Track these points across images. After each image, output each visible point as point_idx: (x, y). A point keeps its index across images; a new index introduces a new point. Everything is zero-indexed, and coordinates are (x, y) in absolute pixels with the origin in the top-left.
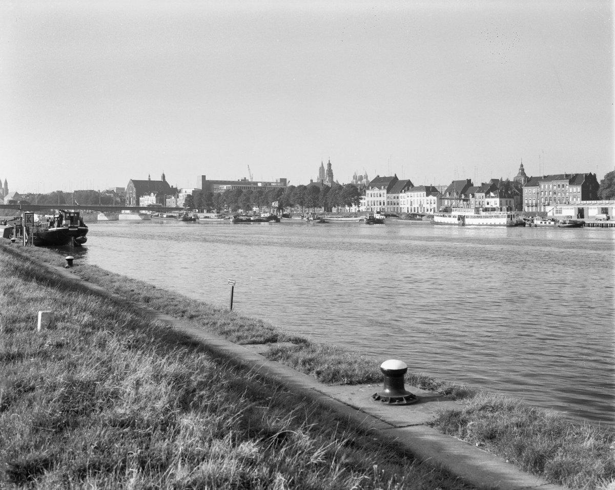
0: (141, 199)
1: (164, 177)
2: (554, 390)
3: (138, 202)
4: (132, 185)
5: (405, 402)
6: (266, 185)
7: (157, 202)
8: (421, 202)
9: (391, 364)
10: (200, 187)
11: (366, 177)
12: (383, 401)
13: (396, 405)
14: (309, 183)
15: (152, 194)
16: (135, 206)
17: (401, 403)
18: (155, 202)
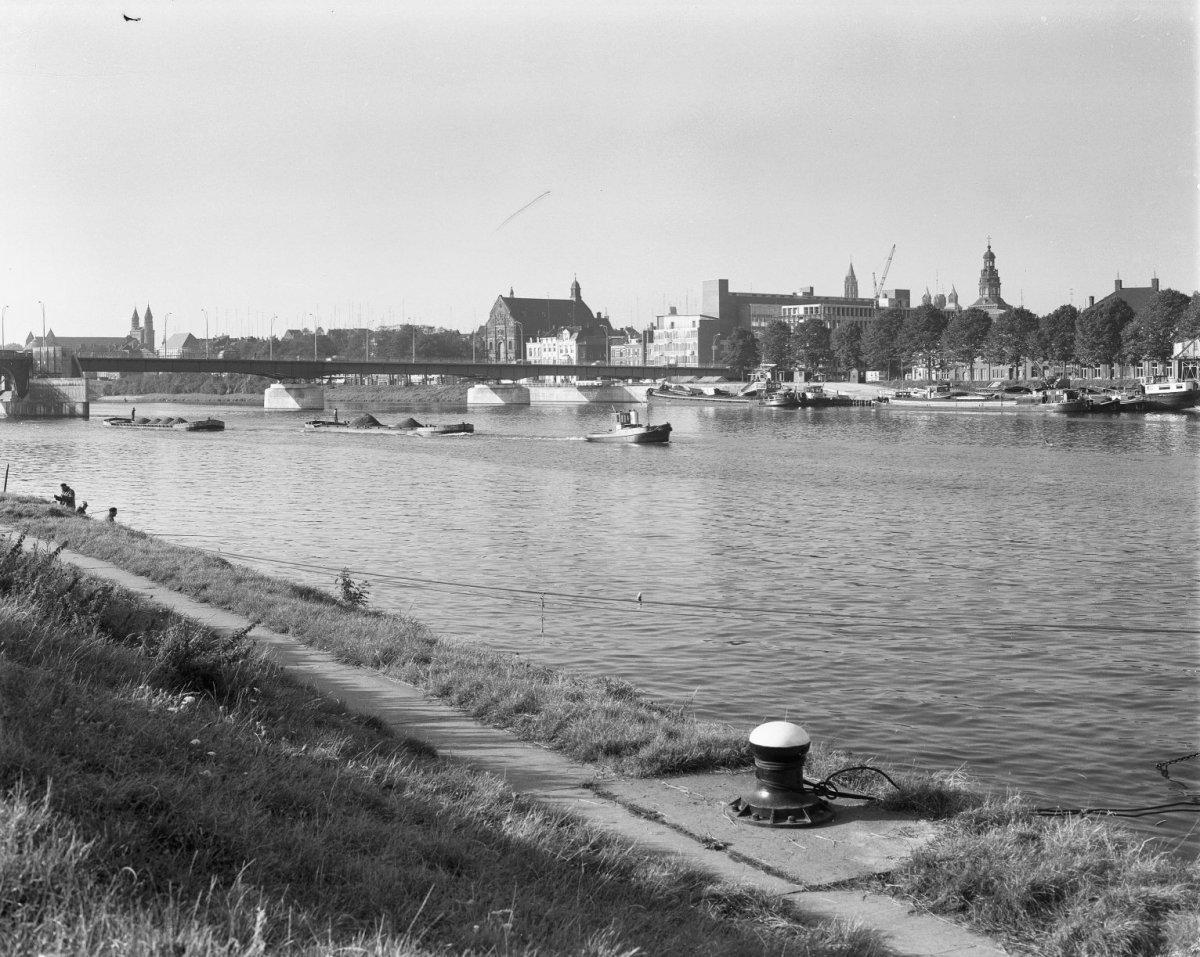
0: (530, 345)
1: (577, 289)
3: (521, 352)
4: (504, 310)
6: (919, 307)
7: (579, 358)
9: (772, 735)
10: (714, 312)
11: (955, 298)
12: (757, 818)
14: (1111, 289)
15: (566, 332)
17: (800, 821)
18: (574, 356)
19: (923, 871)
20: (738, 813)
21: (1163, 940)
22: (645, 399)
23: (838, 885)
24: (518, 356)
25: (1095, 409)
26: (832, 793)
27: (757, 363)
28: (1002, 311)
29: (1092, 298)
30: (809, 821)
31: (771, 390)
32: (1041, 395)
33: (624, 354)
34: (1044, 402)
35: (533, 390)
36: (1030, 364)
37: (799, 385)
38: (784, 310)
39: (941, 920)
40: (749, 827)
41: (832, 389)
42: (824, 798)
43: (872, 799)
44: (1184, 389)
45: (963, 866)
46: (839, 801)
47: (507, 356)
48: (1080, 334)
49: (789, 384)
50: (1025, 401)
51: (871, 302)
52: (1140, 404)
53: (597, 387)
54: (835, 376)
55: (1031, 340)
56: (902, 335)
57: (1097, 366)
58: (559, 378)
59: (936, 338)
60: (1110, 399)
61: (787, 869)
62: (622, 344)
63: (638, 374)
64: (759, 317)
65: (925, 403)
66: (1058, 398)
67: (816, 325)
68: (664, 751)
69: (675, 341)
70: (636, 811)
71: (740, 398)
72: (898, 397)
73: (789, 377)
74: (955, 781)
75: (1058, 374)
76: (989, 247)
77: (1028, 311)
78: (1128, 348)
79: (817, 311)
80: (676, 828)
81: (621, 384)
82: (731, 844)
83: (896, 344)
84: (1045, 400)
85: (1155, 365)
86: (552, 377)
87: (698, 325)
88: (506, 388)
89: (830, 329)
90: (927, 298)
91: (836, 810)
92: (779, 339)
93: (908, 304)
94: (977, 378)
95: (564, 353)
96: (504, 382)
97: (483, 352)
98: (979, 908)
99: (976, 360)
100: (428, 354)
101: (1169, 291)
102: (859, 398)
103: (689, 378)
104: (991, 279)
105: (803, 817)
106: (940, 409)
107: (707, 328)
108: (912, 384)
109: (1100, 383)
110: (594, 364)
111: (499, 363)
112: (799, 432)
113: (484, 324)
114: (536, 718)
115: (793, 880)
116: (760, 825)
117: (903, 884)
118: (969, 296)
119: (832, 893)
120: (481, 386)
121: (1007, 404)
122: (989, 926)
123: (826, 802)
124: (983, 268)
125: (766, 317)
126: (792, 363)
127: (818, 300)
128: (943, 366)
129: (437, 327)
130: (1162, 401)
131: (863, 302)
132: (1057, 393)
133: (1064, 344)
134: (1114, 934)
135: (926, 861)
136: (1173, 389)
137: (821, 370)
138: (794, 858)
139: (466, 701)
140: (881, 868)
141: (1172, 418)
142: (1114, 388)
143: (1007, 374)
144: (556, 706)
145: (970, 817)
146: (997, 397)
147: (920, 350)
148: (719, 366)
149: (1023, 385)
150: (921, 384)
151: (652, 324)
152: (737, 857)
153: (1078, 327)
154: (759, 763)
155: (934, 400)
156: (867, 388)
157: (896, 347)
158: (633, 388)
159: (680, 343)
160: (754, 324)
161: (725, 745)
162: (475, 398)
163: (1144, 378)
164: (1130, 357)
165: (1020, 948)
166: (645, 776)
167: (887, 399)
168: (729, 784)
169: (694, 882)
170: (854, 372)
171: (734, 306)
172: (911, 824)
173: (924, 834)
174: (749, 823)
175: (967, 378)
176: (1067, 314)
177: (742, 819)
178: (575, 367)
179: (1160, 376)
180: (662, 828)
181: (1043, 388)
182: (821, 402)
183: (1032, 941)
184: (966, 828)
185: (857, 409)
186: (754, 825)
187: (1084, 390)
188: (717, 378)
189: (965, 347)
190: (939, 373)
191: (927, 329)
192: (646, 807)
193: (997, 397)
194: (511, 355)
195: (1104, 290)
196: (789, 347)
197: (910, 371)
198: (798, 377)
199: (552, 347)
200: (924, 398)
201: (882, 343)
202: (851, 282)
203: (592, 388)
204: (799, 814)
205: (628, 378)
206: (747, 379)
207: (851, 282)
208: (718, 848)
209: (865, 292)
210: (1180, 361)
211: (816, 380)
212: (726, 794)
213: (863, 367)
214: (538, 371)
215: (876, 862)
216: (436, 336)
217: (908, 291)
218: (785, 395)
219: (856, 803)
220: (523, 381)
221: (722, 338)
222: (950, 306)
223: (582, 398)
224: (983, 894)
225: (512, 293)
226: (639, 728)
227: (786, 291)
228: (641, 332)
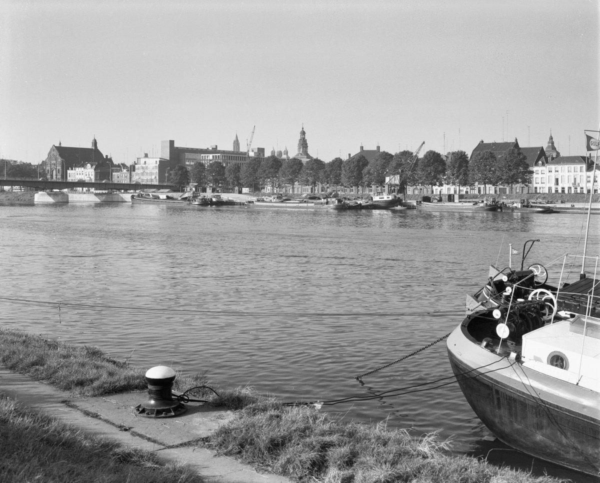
0: (69, 172)
1: (95, 143)
3: (64, 175)
4: (56, 153)
5: (173, 414)
7: (96, 179)
8: (575, 179)
9: (156, 372)
10: (167, 156)
11: (286, 153)
12: (148, 414)
13: (164, 417)
14: (359, 151)
15: (89, 165)
17: (169, 414)
18: (93, 177)
19: (223, 435)
20: (138, 412)
21: (326, 461)
22: (130, 200)
23: (182, 445)
24: (62, 177)
25: (351, 208)
26: (186, 400)
27: (188, 183)
28: (308, 160)
29: (350, 155)
30: (173, 414)
31: (195, 197)
32: (325, 200)
33: (120, 177)
34: (327, 204)
35: (70, 195)
36: (320, 186)
37: (209, 194)
38: (202, 156)
39: (229, 458)
40: (144, 419)
41: (225, 197)
42: (182, 402)
43: (206, 402)
44: (390, 199)
45: (241, 431)
46: (190, 403)
47: (56, 177)
48: (343, 172)
49: (204, 194)
50: (318, 204)
51: (245, 153)
52: (371, 205)
53: (105, 194)
54: (227, 190)
55: (321, 174)
56: (260, 171)
57: (352, 187)
58: (85, 189)
59: (277, 172)
60: (357, 203)
61: (158, 438)
62: (119, 172)
63: (126, 187)
64: (189, 160)
65: (271, 204)
66: (333, 202)
67: (218, 165)
68: (106, 383)
69: (146, 171)
70: (87, 414)
71: (179, 200)
72: (258, 201)
73: (204, 190)
74: (246, 391)
75: (334, 191)
76: (303, 128)
77: (320, 160)
78: (366, 179)
79: (219, 158)
80: (107, 421)
81: (118, 193)
82: (133, 428)
83: (258, 174)
84: (327, 203)
85: (377, 187)
86: (81, 189)
87: (158, 163)
88: (56, 194)
89: (225, 167)
90: (273, 152)
91: (189, 408)
92: (199, 171)
93: (264, 155)
94: (296, 192)
95: (88, 176)
96: (55, 190)
97: (43, 174)
98: (247, 452)
99: (296, 183)
100: (14, 175)
101: (384, 152)
102: (238, 201)
103: (154, 190)
104: (304, 144)
105: (171, 412)
106: (278, 207)
107: (163, 165)
108: (265, 195)
109: (352, 195)
110: (103, 182)
111: (53, 180)
112: (210, 217)
113: (44, 160)
114: (42, 368)
115: (161, 444)
116: (148, 417)
117: (214, 442)
118: (293, 152)
119: (179, 449)
120: (42, 192)
121: (310, 205)
122: (250, 460)
123: (183, 405)
124: (299, 138)
125: (193, 160)
126: (206, 183)
127: (219, 152)
128: (280, 186)
129: (19, 161)
130: (380, 204)
131: (242, 153)
132: (333, 200)
133: (336, 176)
134: (305, 460)
135: (225, 432)
136: (385, 199)
137: (220, 187)
138: (163, 433)
139: (7, 360)
140: (204, 436)
141: (384, 212)
142: (359, 198)
143: (310, 190)
144: (52, 362)
145: (251, 408)
146: (305, 202)
147: (269, 178)
148: (169, 184)
149: (317, 196)
150: (269, 195)
151: (135, 162)
152: (135, 434)
153: (343, 168)
154: (150, 387)
155: (275, 202)
156: (244, 196)
157: (257, 176)
158: (124, 195)
159: (149, 172)
160: (187, 163)
161: (138, 378)
162: (38, 199)
163: (373, 193)
164: (366, 183)
165: (263, 469)
166: (95, 396)
167: (253, 202)
168: (138, 398)
169: (108, 447)
170: (237, 188)
171: (177, 154)
172: (223, 413)
173: (228, 418)
174: (144, 417)
175: (291, 192)
176: (338, 162)
177: (140, 415)
178: (94, 183)
179: (380, 193)
180: (99, 421)
181: (326, 197)
182: (220, 203)
183: (269, 465)
184: (248, 414)
185: (237, 206)
186: (146, 417)
187: (345, 198)
188: (168, 190)
189: (290, 177)
190: (278, 189)
191: (272, 168)
192: (93, 412)
193: (305, 202)
194: (59, 176)
195: (355, 151)
196: (204, 175)
197: (264, 188)
198: (209, 190)
199: (81, 173)
200: (271, 202)
201: (250, 174)
202: (237, 143)
203: (103, 194)
204: (168, 411)
205: (122, 189)
206: (183, 191)
207: (237, 143)
208: (126, 430)
209: (243, 149)
210: (389, 185)
211: (218, 192)
212: (135, 403)
213: (241, 186)
214: (73, 185)
215: (203, 432)
216: (18, 166)
217: (264, 149)
218: (202, 199)
219: (198, 404)
220: (65, 190)
221: (171, 170)
222: (284, 157)
223: (97, 200)
224: (249, 445)
225: (60, 144)
226: (95, 371)
227: (204, 147)
228: (129, 166)
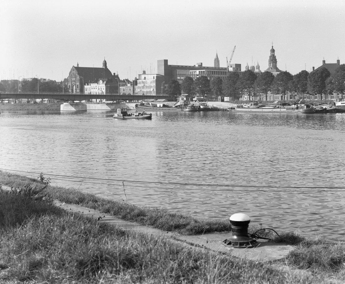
0: (86, 87)
1: (105, 63)
2: (143, 198)
3: (82, 90)
4: (75, 72)
10: (162, 73)
12: (233, 245)
14: (321, 64)
16: (79, 94)
18: (104, 91)
76: (272, 47)
88: (77, 104)
